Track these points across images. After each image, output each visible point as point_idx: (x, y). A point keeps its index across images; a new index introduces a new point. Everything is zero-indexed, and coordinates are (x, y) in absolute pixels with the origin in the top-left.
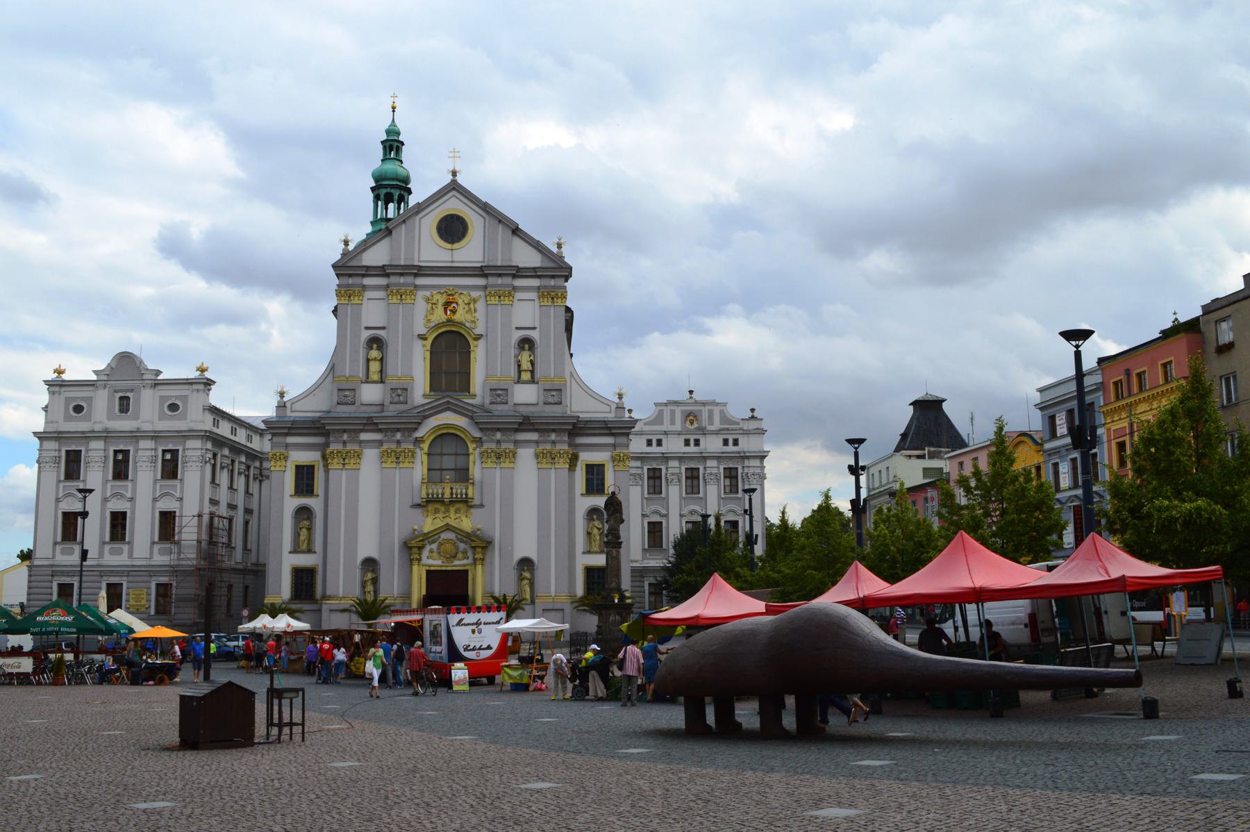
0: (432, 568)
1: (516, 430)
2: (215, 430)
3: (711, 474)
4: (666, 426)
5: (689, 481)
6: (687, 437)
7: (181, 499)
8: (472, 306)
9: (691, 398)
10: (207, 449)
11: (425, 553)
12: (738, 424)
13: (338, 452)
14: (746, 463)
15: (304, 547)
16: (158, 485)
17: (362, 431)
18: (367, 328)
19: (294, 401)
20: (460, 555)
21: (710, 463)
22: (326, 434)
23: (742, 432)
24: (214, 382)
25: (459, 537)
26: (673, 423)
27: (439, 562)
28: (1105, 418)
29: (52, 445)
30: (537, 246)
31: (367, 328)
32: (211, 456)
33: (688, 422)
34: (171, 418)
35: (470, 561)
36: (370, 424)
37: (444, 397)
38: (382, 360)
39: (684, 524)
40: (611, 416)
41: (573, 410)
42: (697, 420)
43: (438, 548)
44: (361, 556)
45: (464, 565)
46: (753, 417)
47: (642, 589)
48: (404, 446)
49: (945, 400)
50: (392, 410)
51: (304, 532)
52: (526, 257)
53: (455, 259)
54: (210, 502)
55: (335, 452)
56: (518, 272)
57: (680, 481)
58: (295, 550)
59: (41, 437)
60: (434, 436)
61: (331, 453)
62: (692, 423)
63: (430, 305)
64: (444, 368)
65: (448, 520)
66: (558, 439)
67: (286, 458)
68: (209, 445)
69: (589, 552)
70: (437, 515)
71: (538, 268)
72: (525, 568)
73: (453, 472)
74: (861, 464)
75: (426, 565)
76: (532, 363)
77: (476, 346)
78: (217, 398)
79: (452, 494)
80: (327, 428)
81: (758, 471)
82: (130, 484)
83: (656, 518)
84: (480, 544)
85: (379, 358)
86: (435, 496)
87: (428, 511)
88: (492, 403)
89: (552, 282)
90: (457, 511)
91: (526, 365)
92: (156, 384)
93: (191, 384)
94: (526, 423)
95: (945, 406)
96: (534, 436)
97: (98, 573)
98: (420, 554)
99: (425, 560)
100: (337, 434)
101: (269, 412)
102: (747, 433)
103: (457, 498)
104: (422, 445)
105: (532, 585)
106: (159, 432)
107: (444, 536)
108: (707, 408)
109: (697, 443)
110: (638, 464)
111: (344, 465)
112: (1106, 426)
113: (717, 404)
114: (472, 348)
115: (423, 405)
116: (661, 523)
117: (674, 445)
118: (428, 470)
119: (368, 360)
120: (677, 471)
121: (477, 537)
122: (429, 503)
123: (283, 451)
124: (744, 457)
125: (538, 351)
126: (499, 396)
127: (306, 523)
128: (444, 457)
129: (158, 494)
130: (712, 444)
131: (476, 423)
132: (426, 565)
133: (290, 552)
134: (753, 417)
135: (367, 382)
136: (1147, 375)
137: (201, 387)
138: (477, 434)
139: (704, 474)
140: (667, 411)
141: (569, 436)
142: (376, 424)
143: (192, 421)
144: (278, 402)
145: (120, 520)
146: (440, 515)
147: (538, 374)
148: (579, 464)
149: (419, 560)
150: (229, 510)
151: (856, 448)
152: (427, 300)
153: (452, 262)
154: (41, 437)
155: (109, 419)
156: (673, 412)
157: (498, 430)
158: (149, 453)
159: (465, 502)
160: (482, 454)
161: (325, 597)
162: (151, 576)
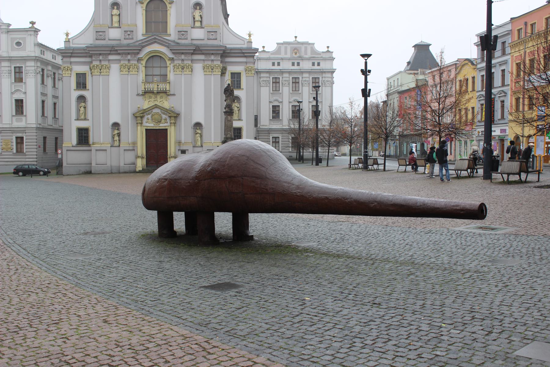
0: (148, 128)
1: (192, 54)
2: (42, 56)
3: (305, 81)
4: (282, 55)
6: (293, 61)
9: (296, 40)
10: (37, 66)
11: (145, 120)
12: (320, 54)
14: (324, 75)
15: (83, 117)
16: (13, 86)
17: (109, 54)
19: (73, 38)
20: (163, 121)
21: (305, 75)
22: (91, 56)
23: (322, 59)
24: (40, 30)
25: (163, 111)
26: (286, 53)
27: (152, 125)
28: (511, 50)
32: (41, 70)
35: (168, 124)
36: (113, 50)
37: (153, 36)
38: (119, 15)
39: (291, 107)
40: (245, 46)
41: (224, 43)
42: (299, 52)
43: (152, 117)
44: (112, 121)
46: (328, 51)
47: (268, 140)
48: (132, 62)
49: (430, 45)
57: (289, 84)
60: (148, 57)
61: (93, 66)
62: (296, 54)
64: (153, 20)
65: (156, 103)
66: (215, 58)
70: (150, 100)
72: (198, 128)
73: (159, 77)
74: (368, 69)
75: (145, 126)
76: (201, 17)
77: (170, 7)
78: (41, 39)
79: (158, 88)
80: (90, 52)
81: (330, 79)
83: (276, 104)
84: (175, 116)
85: (118, 14)
87: (145, 97)
88: (179, 39)
90: (161, 97)
91: (198, 18)
92: (8, 31)
93: (27, 31)
95: (430, 48)
96: (202, 57)
98: (142, 120)
99: (145, 124)
100: (96, 56)
101: (62, 45)
102: (325, 59)
103: (150, 90)
104: (142, 62)
105: (201, 136)
106: (11, 57)
107: (156, 111)
108: (305, 46)
109: (298, 64)
110: (267, 75)
112: (511, 54)
113: (310, 44)
114: (168, 8)
115: (142, 40)
116: (279, 106)
117: (286, 65)
118: (146, 75)
119: (112, 15)
120: (288, 79)
121: (172, 111)
122: (146, 92)
123: (69, 65)
124: (322, 72)
126: (183, 35)
127: (83, 104)
128: (162, 68)
129: (13, 90)
130: (306, 65)
131: (171, 50)
133: (75, 120)
134: (328, 51)
136: (536, 25)
137: (33, 33)
138: (171, 56)
139: (302, 81)
141: (221, 57)
142: (117, 50)
144: (65, 39)
146: (152, 100)
147: (204, 23)
149: (141, 123)
150: (53, 99)
151: (366, 60)
156: (286, 48)
157: (183, 53)
158: (7, 69)
159: (165, 93)
160: (174, 66)
161: (93, 144)
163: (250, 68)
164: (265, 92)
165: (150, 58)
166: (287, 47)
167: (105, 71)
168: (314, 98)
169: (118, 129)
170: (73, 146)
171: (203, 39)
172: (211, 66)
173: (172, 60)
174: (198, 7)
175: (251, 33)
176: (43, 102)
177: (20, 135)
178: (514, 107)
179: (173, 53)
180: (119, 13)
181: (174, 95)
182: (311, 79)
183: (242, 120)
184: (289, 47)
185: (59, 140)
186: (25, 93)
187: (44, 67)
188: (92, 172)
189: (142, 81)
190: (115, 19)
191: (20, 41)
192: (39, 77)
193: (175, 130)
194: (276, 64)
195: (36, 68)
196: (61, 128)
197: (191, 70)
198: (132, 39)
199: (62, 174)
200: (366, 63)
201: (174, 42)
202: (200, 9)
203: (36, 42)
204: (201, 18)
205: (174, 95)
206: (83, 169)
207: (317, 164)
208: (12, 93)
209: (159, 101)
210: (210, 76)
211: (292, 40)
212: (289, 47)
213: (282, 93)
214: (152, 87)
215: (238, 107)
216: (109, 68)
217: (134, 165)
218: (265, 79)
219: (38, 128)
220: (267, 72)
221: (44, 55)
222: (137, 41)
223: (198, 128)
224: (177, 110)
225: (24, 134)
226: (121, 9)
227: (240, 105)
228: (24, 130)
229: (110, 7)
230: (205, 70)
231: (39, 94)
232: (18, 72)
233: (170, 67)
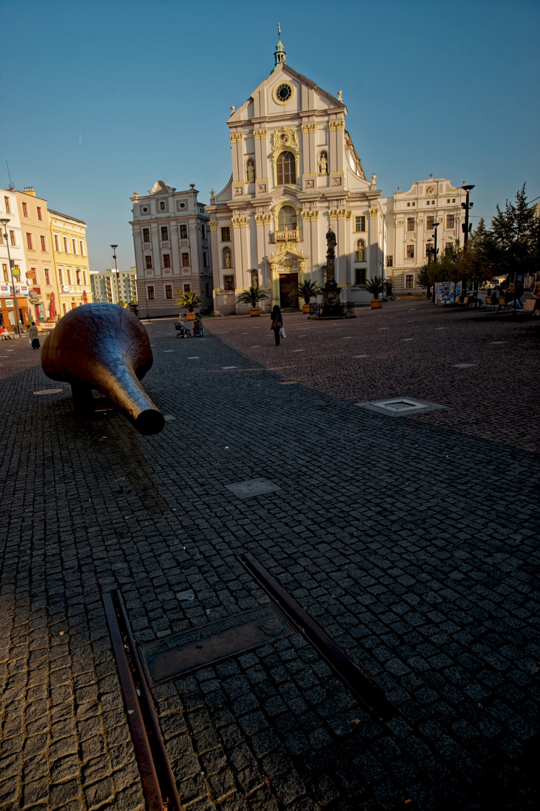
2: (202, 214)
15: (228, 265)
29: (137, 227)
51: (227, 259)
58: (225, 267)
67: (217, 225)
68: (199, 221)
69: (357, 262)
74: (470, 202)
82: (169, 242)
83: (411, 243)
91: (324, 166)
109: (433, 203)
148: (352, 216)
155: (157, 213)
168: (433, 236)
176: (205, 254)
178: (216, 234)
186: (171, 249)
187: (203, 224)
188: (237, 312)
192: (200, 233)
200: (468, 196)
206: (229, 311)
220: (402, 213)
228: (190, 278)
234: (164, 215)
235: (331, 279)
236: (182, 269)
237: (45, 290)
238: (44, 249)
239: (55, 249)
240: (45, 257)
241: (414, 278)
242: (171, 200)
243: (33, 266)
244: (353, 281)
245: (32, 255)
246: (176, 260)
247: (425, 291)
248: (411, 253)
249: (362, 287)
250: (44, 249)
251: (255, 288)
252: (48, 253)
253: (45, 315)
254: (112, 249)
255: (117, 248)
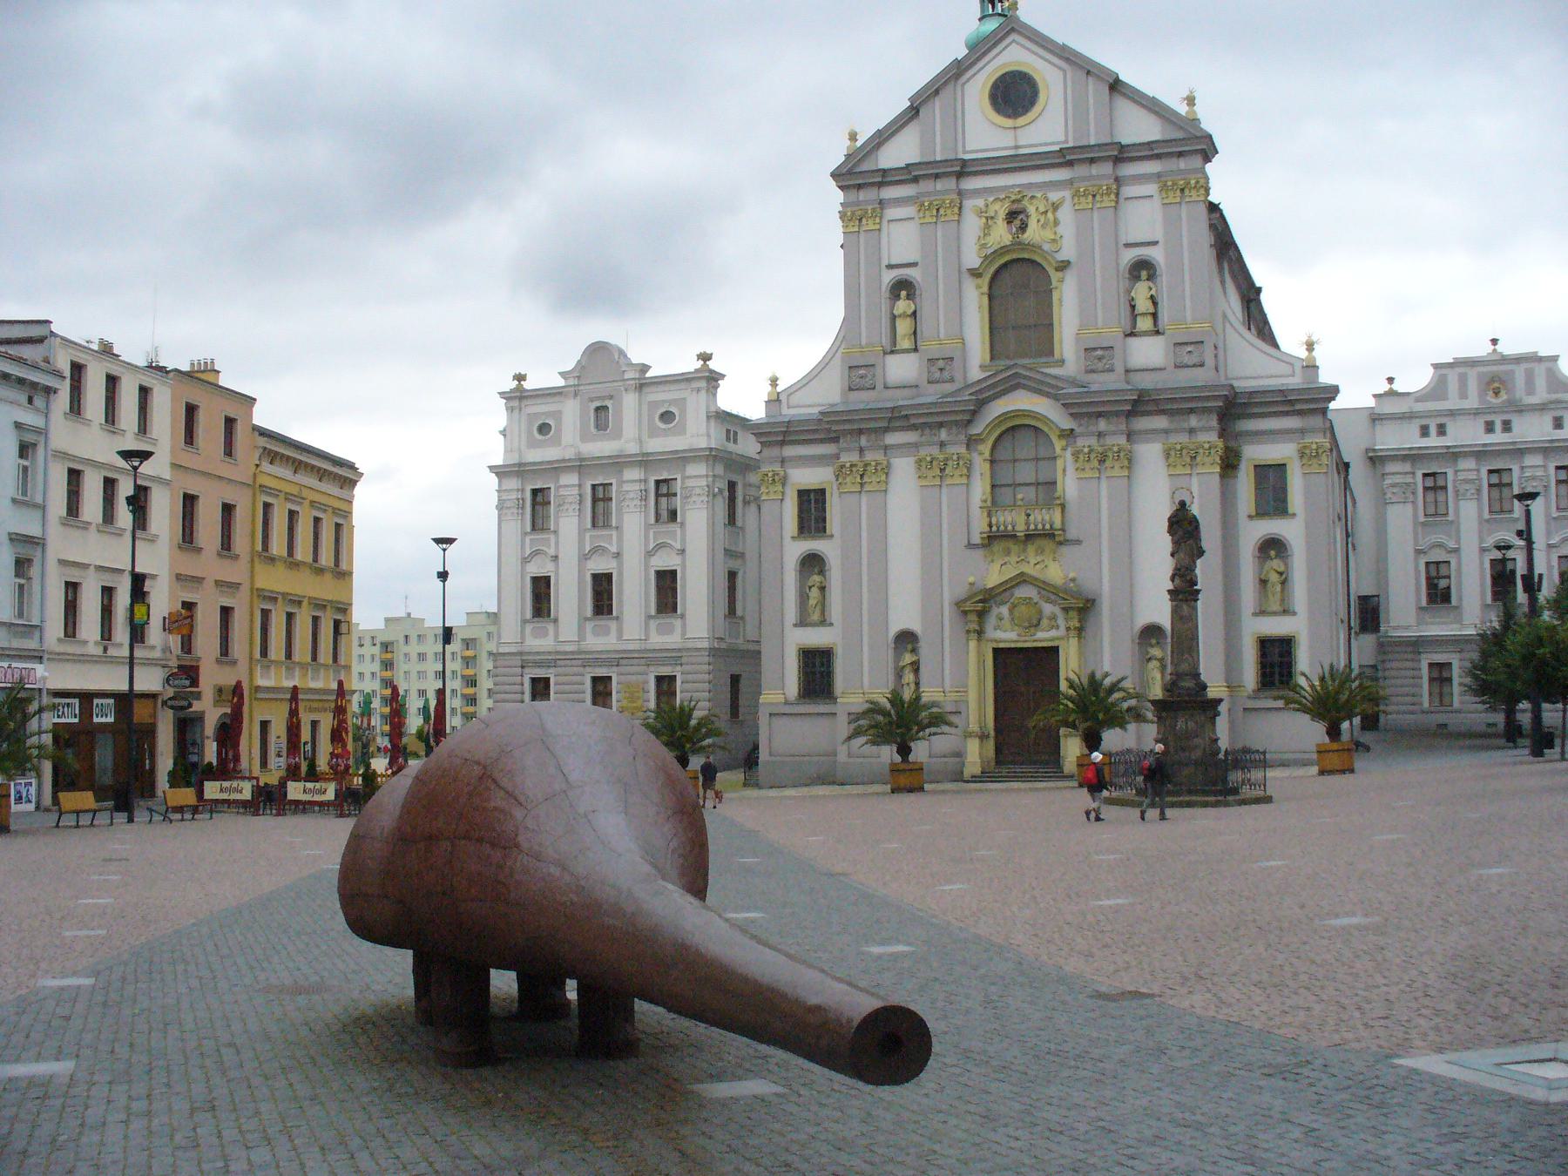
0: (1002, 645)
2: (731, 447)
4: (1453, 403)
5: (1495, 493)
6: (1489, 418)
7: (682, 552)
8: (1050, 215)
9: (1495, 350)
11: (991, 621)
13: (851, 466)
15: (816, 617)
17: (887, 430)
18: (890, 267)
20: (1045, 622)
21: (1529, 460)
22: (835, 440)
27: (1012, 635)
29: (513, 483)
30: (1153, 106)
31: (890, 267)
33: (1491, 393)
34: (665, 433)
35: (1062, 632)
36: (897, 419)
37: (1008, 368)
39: (1555, 562)
41: (1230, 376)
43: (1011, 611)
44: (894, 629)
45: (1052, 640)
50: (931, 395)
51: (815, 593)
52: (1137, 128)
53: (1021, 143)
54: (726, 554)
55: (848, 465)
56: (1121, 154)
57: (1479, 491)
59: (500, 472)
60: (996, 434)
62: (1497, 393)
63: (984, 220)
65: (1028, 569)
67: (784, 483)
68: (720, 470)
70: (1006, 559)
71: (1152, 142)
73: (1033, 489)
75: (991, 641)
77: (1061, 281)
79: (1027, 524)
83: (1437, 556)
84: (1083, 608)
85: (910, 312)
86: (1002, 528)
89: (1182, 164)
90: (1040, 551)
91: (1143, 305)
94: (1141, 404)
96: (1161, 422)
97: (580, 662)
103: (1044, 529)
104: (981, 447)
106: (648, 454)
108: (1524, 366)
109: (1507, 426)
110: (1407, 467)
111: (862, 485)
113: (1540, 359)
114: (1054, 283)
117: (1466, 434)
119: (894, 318)
120: (1472, 476)
122: (995, 539)
125: (1164, 279)
127: (816, 578)
128: (1041, 463)
132: (991, 641)
133: (795, 625)
135: (892, 352)
138: (1067, 423)
140: (1453, 377)
143: (692, 436)
145: (605, 584)
146: (1013, 559)
149: (980, 633)
152: (980, 213)
153: (1017, 147)
154: (500, 472)
156: (1463, 380)
158: (637, 487)
160: (1076, 455)
162: (648, 665)
163: (1314, 446)
164: (1402, 520)
165: (1000, 436)
166: (1466, 374)
167: (874, 479)
169: (914, 651)
170: (787, 703)
171: (1162, 366)
172: (1186, 448)
173: (1069, 435)
174: (1144, 274)
175: (1314, 338)
176: (732, 575)
177: (665, 671)
179: (1071, 414)
180: (913, 308)
181: (1078, 542)
182: (1552, 471)
183: (1294, 613)
184: (1472, 374)
185: (744, 685)
187: (734, 478)
189: (980, 504)
190: (903, 327)
191: (672, 409)
193: (1080, 647)
194: (1433, 430)
195: (710, 479)
196: (752, 647)
197: (1126, 463)
198: (952, 380)
199: (757, 785)
201: (1073, 382)
202: (1151, 278)
203: (713, 409)
204: (1155, 304)
205: (1078, 542)
207: (1537, 752)
208: (649, 554)
209: (1033, 561)
210: (1187, 478)
211: (1482, 350)
212: (1472, 374)
213: (1455, 524)
214: (1009, 519)
215: (1281, 574)
216: (887, 469)
217: (958, 759)
218: (1398, 479)
219: (714, 649)
220: (1405, 458)
221: (735, 441)
222: (968, 386)
223: (1154, 641)
224: (1088, 584)
225: (679, 668)
226: (918, 299)
227: (1286, 565)
228: (675, 656)
229: (888, 295)
230: (1171, 460)
231: (720, 555)
232: (664, 495)
233: (1066, 461)
234: (602, 447)
235: (1184, 667)
236: (529, 628)
237: (212, 676)
238: (226, 543)
239: (259, 547)
240: (234, 572)
241: (1456, 672)
242: (630, 401)
243: (189, 598)
244: (1250, 675)
245: (191, 566)
246: (634, 594)
247: (1499, 718)
248: (1439, 594)
249: (1288, 701)
250: (226, 543)
251: (907, 695)
252: (237, 557)
253: (201, 754)
254: (437, 549)
255: (452, 548)
